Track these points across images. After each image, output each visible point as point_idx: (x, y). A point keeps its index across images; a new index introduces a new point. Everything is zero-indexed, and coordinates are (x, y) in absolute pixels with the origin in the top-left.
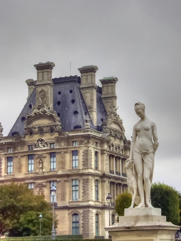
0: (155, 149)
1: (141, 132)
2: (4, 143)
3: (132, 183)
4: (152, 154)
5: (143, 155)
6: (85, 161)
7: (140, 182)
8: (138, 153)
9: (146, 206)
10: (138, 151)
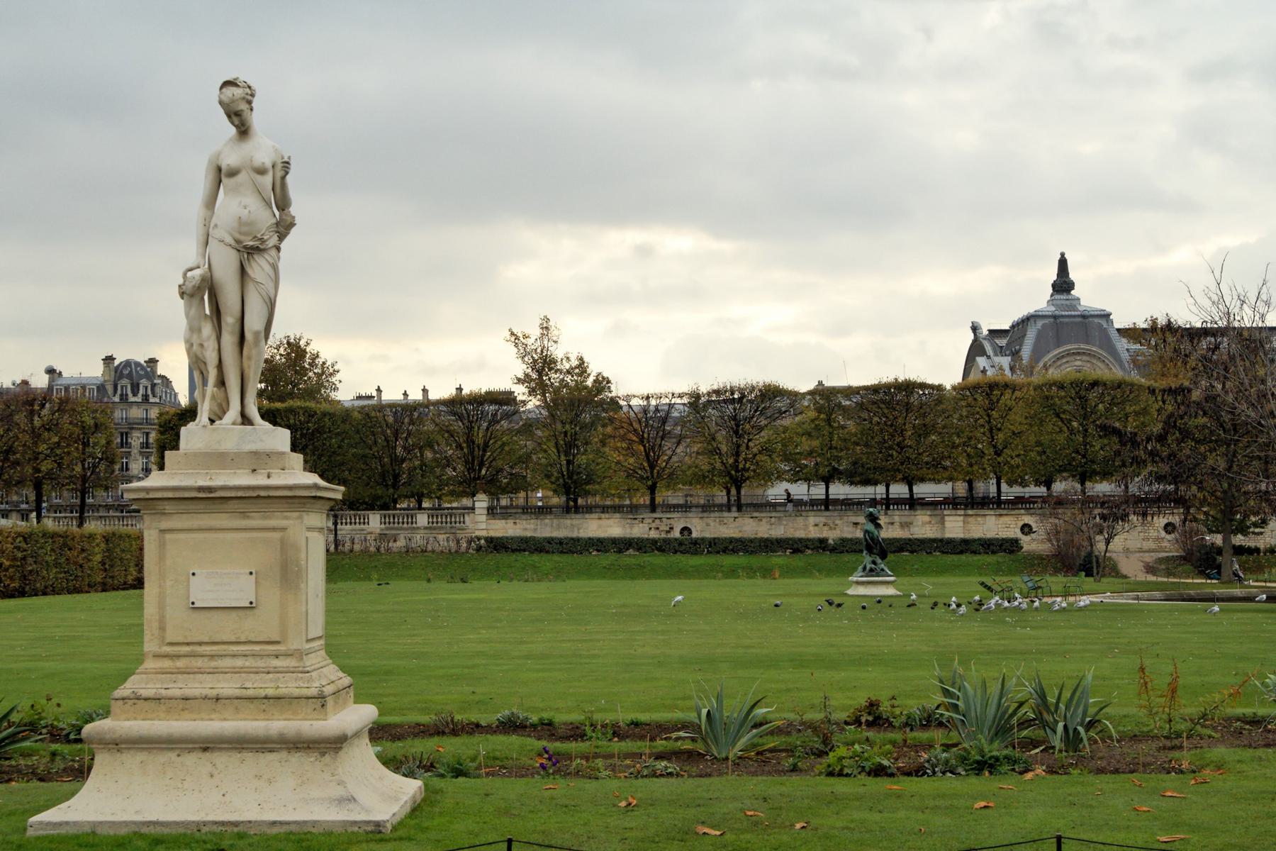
1: (241, 177)
2: (1139, 542)
3: (202, 345)
4: (273, 252)
7: (229, 340)
9: (245, 420)
10: (229, 240)
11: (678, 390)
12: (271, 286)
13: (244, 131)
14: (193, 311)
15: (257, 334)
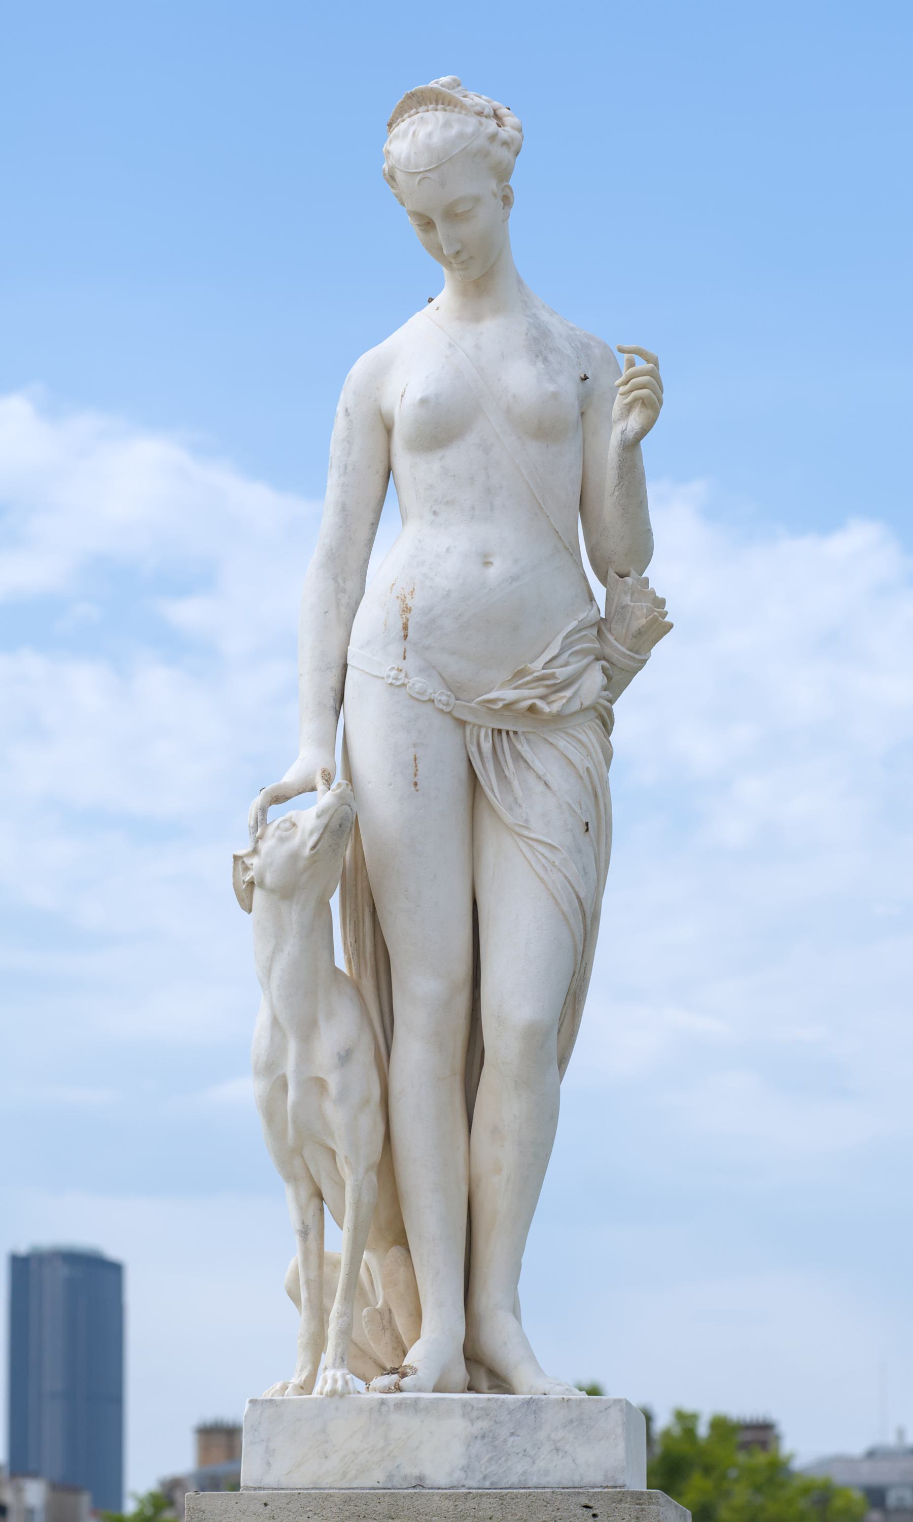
4: (589, 734)
6: (585, 776)
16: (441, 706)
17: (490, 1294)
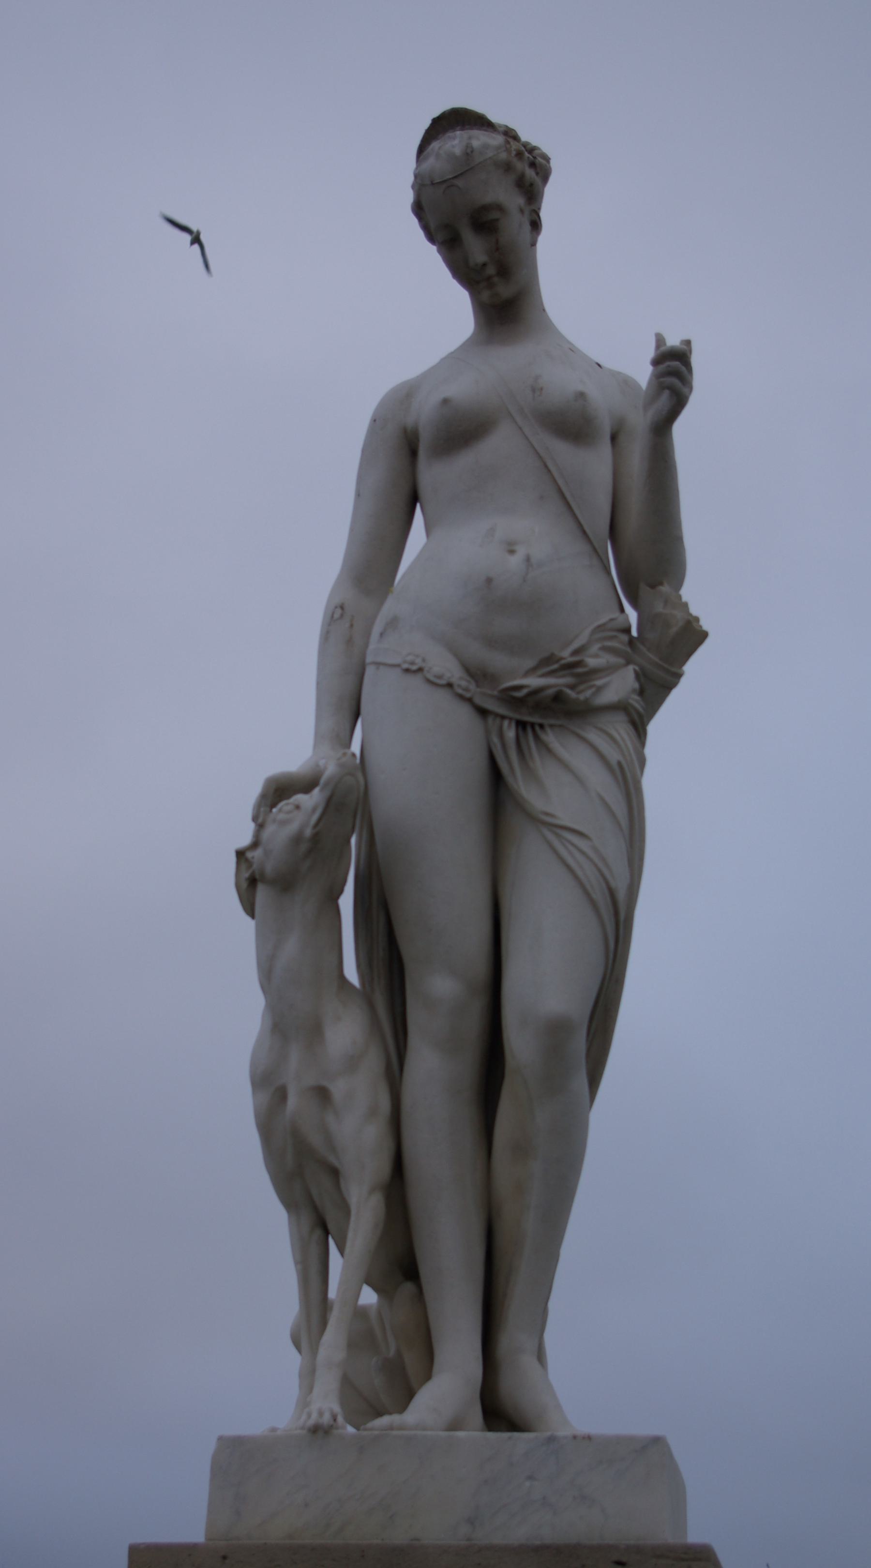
0: (657, 685)
1: (499, 444)
3: (322, 1094)
4: (621, 729)
5: (510, 734)
6: (616, 767)
7: (435, 1072)
8: (470, 700)
10: (443, 664)
11: (286, 1300)
12: (613, 849)
13: (502, 295)
14: (291, 947)
15: (556, 1031)
16: (460, 691)
17: (513, 1337)
